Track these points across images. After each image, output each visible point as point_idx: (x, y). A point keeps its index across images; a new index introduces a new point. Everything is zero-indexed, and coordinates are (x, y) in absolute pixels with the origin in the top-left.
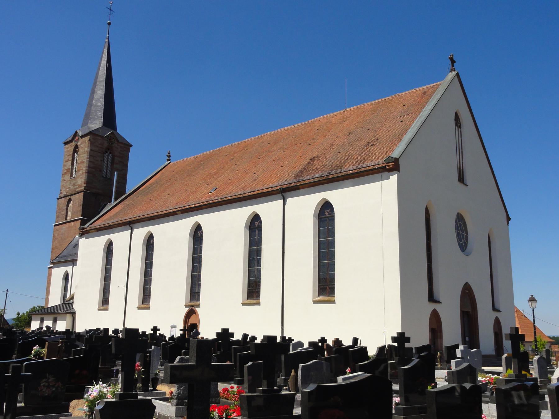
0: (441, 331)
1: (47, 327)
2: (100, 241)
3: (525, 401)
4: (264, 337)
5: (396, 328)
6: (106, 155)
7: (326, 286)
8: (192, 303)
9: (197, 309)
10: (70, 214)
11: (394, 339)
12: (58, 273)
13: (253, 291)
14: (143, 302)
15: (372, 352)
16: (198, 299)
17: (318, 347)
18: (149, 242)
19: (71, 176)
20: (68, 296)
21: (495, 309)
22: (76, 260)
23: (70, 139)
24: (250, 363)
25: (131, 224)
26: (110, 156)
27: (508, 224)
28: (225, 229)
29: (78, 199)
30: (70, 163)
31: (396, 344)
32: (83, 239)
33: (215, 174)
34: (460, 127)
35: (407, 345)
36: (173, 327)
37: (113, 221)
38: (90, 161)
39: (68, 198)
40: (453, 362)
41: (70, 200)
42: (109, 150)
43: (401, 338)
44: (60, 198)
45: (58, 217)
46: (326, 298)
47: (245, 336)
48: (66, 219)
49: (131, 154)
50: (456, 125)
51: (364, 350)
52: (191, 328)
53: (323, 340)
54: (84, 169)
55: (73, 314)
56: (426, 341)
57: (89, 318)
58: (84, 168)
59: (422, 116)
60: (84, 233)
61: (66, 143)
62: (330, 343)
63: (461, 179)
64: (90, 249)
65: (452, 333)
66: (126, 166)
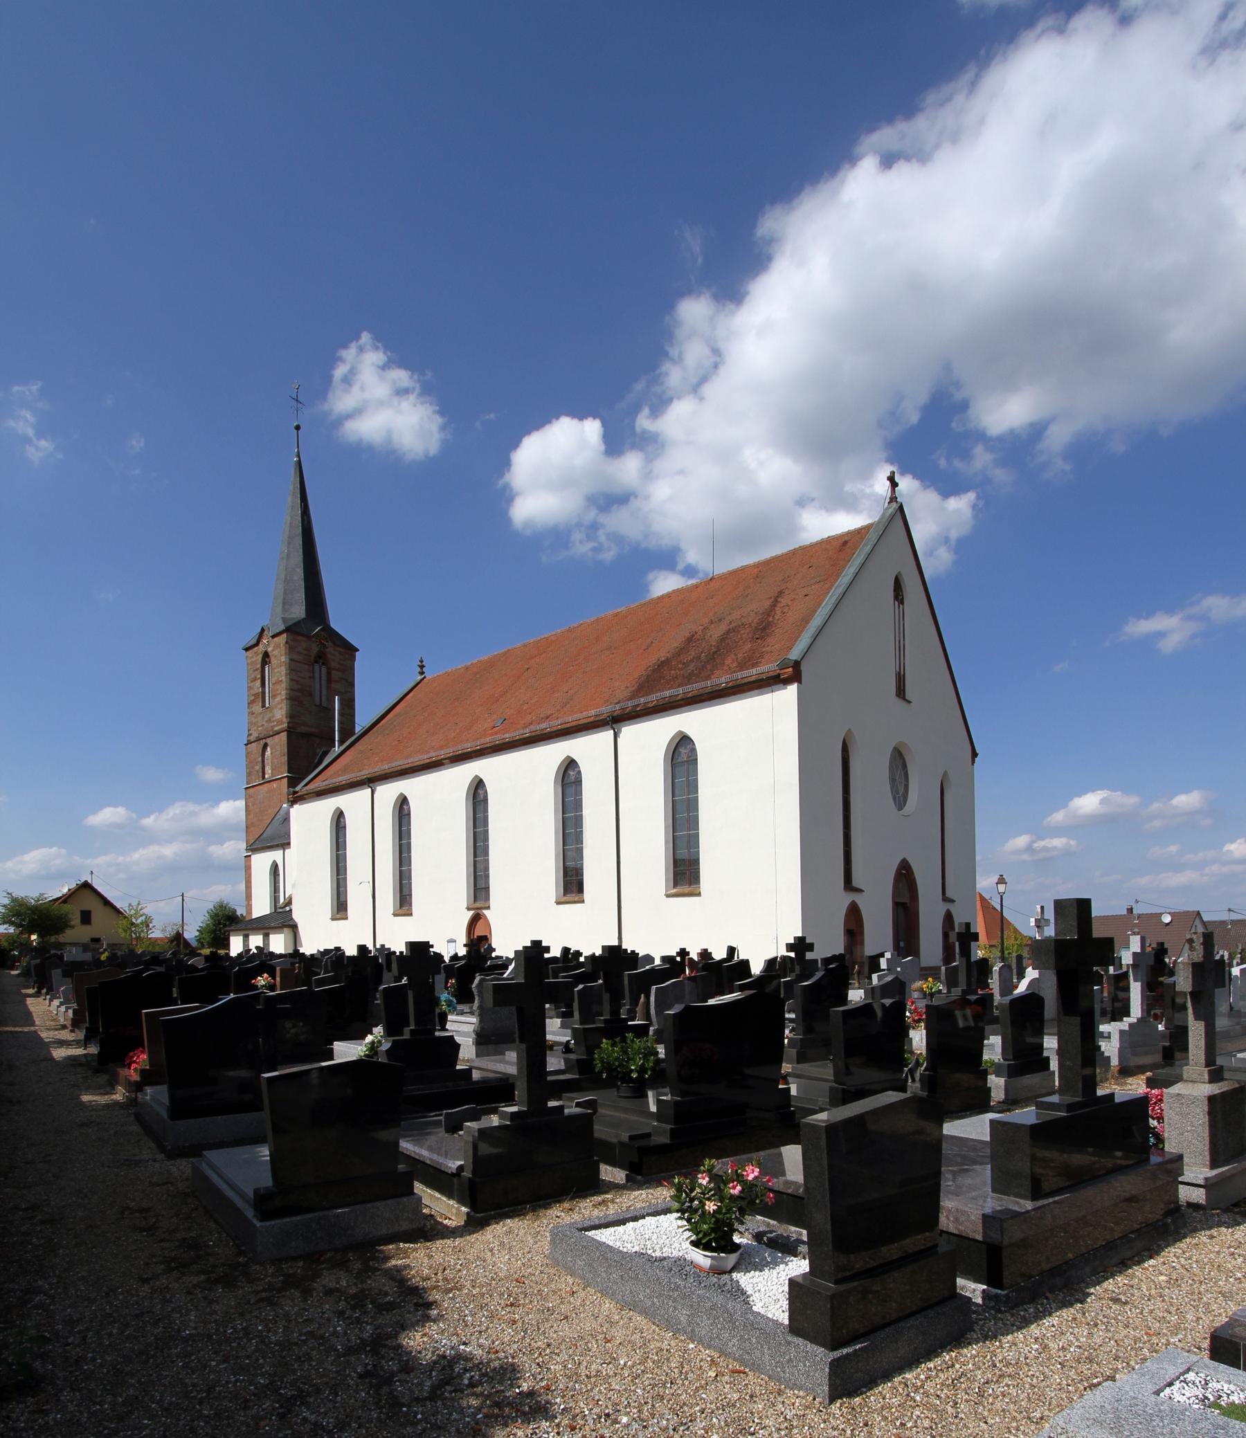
0: (862, 933)
1: (257, 948)
2: (323, 809)
3: (972, 1024)
4: (603, 947)
5: (794, 930)
6: (317, 667)
7: (684, 873)
8: (478, 905)
9: (485, 912)
10: (268, 770)
11: (790, 947)
12: (262, 862)
13: (572, 884)
14: (401, 906)
15: (757, 968)
16: (487, 898)
17: (676, 964)
18: (402, 808)
19: (264, 706)
20: (282, 900)
21: (946, 899)
22: (289, 844)
23: (254, 642)
24: (581, 987)
25: (371, 781)
26: (324, 669)
27: (973, 762)
28: (521, 780)
29: (279, 743)
30: (258, 683)
31: (792, 955)
32: (296, 807)
33: (501, 696)
34: (902, 602)
35: (809, 956)
36: (452, 941)
37: (343, 779)
38: (292, 680)
39: (262, 742)
40: (875, 977)
41: (265, 746)
42: (321, 658)
43: (800, 946)
44: (249, 743)
45: (249, 775)
46: (686, 889)
47: (566, 950)
48: (263, 777)
49: (357, 665)
50: (896, 598)
51: (745, 964)
52: (478, 944)
53: (683, 953)
54: (284, 693)
55: (294, 927)
56: (839, 949)
57: (319, 934)
58: (283, 693)
59: (839, 586)
60: (296, 799)
61: (247, 649)
62: (694, 955)
63: (901, 692)
64: (309, 821)
65: (879, 936)
66: (352, 685)
